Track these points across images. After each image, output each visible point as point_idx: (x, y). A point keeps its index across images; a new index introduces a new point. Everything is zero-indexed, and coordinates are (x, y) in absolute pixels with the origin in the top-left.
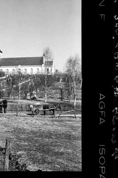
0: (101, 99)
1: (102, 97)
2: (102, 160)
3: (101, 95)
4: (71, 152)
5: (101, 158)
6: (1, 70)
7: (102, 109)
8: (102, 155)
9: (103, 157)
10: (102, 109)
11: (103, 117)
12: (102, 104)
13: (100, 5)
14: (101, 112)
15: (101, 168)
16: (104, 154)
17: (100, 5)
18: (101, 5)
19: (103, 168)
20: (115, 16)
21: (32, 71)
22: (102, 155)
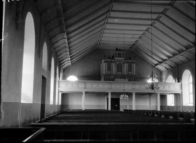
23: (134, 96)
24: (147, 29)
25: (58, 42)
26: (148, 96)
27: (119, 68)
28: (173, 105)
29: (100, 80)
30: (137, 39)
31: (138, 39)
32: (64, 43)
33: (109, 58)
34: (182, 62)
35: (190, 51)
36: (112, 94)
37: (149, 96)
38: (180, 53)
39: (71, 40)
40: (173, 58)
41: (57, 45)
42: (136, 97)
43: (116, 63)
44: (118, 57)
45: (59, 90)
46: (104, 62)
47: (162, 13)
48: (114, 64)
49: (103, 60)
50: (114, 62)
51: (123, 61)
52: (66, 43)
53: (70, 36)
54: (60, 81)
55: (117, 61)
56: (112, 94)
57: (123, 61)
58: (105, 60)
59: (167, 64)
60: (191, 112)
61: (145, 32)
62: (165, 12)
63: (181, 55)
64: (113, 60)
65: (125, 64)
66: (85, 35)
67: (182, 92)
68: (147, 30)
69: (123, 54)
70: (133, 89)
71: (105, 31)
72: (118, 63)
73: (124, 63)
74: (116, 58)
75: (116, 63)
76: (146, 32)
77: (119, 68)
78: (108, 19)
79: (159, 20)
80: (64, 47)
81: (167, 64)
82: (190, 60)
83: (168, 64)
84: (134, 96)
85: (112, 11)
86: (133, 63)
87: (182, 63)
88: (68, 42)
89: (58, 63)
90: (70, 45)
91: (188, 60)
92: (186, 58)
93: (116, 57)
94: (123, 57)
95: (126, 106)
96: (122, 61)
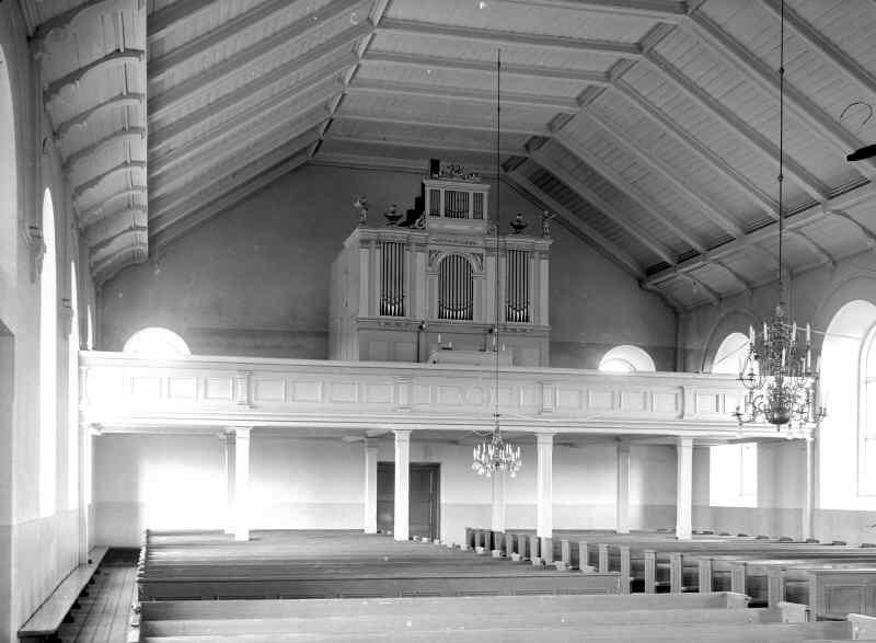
23: (545, 451)
24: (585, 92)
25: (101, 183)
26: (612, 449)
27: (455, 279)
28: (751, 501)
29: (324, 353)
30: (565, 109)
31: (571, 104)
32: (121, 97)
33: (393, 219)
34: (715, 293)
35: (800, 228)
36: (417, 438)
37: (618, 451)
38: (831, 202)
39: (173, 75)
40: (822, 214)
41: (93, 194)
42: (557, 459)
43: (437, 253)
44: (446, 215)
45: (81, 417)
46: (365, 242)
47: (639, 48)
48: (421, 258)
49: (357, 234)
50: (422, 246)
51: (480, 243)
52: (135, 96)
53: (162, 82)
54: (87, 362)
55: (439, 242)
56: (417, 438)
57: (480, 243)
58: (371, 233)
59: (848, 217)
60: (740, 535)
61: (626, 55)
62: (563, 126)
63: (838, 212)
64: (417, 236)
65: (490, 261)
66: (259, 53)
67: (814, 433)
68: (647, 46)
69: (479, 197)
70: (539, 413)
71: (384, 40)
72: (446, 252)
73: (481, 256)
74: (433, 223)
75: (437, 253)
76: (606, 85)
77: (455, 279)
78: (377, 31)
79: (697, 8)
80: (126, 205)
81: (848, 217)
82: (836, 258)
83: (855, 218)
84: (545, 451)
85: (385, 22)
86: (536, 255)
87: (711, 297)
88: (150, 87)
89: (49, 164)
90: (159, 115)
91: (744, 287)
92: (737, 276)
93: (435, 213)
94: (478, 215)
95: (485, 510)
96: (472, 244)
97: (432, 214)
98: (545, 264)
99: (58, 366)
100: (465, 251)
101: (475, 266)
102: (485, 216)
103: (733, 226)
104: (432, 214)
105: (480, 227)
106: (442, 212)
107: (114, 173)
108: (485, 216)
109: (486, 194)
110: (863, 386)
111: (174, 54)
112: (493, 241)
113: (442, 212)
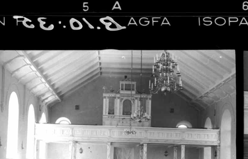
0: (135, 23)
1: (132, 22)
2: (220, 21)
3: (242, 22)
4: (168, 82)
5: (141, 22)
6: (47, 105)
7: (149, 22)
8: (213, 22)
9: (217, 19)
10: (149, 22)
11: (160, 21)
12: (143, 22)
13: (4, 24)
14: (231, 23)
15: (154, 23)
16: (211, 18)
17: (4, 24)
18: (3, 22)
19: (231, 20)
20: (84, 11)
21: (107, 97)
22: (213, 22)
43: (122, 99)
48: (119, 100)
65: (136, 101)
72: (125, 98)
97: (122, 90)
98: (150, 101)
99: (20, 125)
100: (130, 98)
101: (132, 102)
102: (135, 89)
103: (175, 152)
104: (122, 90)
105: (134, 92)
106: (124, 89)
107: (23, 68)
108: (135, 89)
109: (135, 84)
110: (106, 143)
111: (95, 78)
112: (139, 96)
113: (124, 89)
